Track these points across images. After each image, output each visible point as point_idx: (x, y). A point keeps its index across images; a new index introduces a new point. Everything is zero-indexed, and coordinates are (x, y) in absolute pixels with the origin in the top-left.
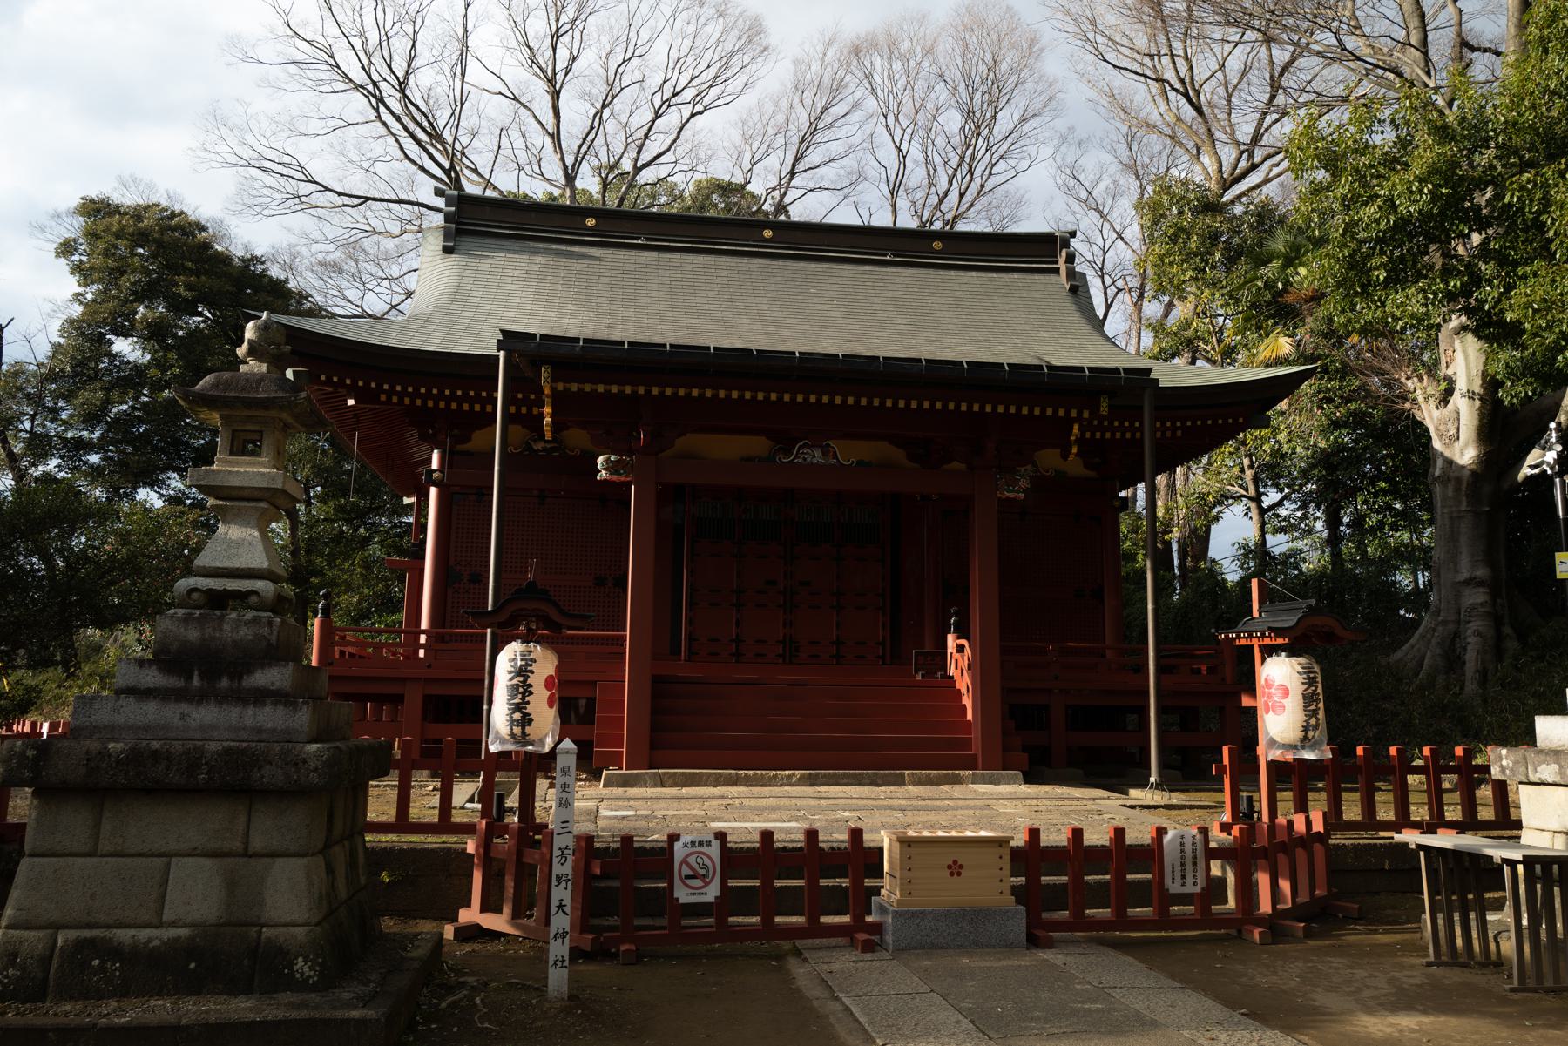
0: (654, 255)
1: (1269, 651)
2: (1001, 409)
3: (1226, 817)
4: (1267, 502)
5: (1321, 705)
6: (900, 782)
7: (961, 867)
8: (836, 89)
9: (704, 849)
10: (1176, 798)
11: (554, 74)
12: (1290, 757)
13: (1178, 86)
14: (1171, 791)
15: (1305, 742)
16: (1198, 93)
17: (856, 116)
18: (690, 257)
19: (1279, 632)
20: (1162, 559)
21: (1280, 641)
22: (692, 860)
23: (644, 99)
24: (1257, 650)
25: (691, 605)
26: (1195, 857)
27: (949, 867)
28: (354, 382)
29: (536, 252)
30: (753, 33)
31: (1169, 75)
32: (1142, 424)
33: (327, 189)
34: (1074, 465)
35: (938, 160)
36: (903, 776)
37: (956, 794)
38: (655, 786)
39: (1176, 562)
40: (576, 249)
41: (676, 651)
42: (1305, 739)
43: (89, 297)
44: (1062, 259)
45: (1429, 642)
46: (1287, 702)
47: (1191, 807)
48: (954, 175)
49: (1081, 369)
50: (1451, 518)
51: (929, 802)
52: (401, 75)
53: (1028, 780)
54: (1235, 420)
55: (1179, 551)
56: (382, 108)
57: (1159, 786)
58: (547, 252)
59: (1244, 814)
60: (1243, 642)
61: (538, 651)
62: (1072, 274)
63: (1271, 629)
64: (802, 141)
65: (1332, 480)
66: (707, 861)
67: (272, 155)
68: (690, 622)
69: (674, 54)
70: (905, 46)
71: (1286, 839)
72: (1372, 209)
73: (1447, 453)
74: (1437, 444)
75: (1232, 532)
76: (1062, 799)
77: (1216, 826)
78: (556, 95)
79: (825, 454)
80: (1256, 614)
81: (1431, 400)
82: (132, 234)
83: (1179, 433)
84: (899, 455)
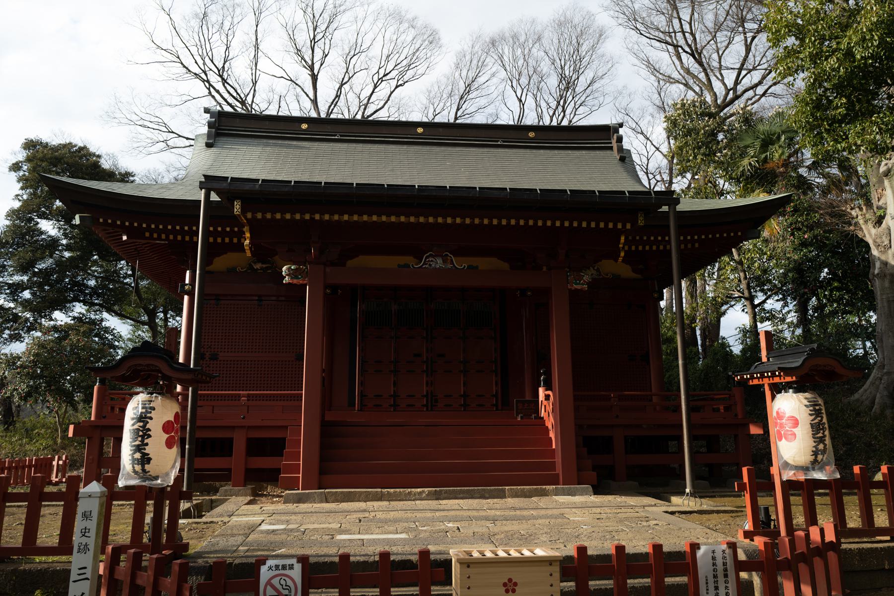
0: (345, 145)
1: (777, 389)
2: (567, 224)
3: (748, 526)
4: (756, 302)
5: (827, 433)
6: (502, 495)
7: (515, 584)
8: (481, 66)
9: (287, 572)
10: (706, 504)
11: (313, 64)
12: (802, 477)
13: (688, 49)
14: (701, 497)
15: (815, 464)
16: (700, 54)
17: (495, 80)
18: (369, 146)
19: (787, 371)
20: (689, 341)
21: (788, 379)
22: (275, 582)
23: (369, 80)
24: (767, 388)
25: (363, 371)
26: (726, 570)
27: (505, 585)
28: (123, 223)
29: (267, 145)
30: (433, 39)
31: (682, 42)
32: (670, 238)
33: (180, 136)
34: (624, 270)
35: (543, 105)
36: (504, 491)
37: (541, 505)
38: (321, 502)
39: (699, 342)
40: (295, 143)
41: (352, 404)
42: (815, 462)
43: (25, 197)
44: (614, 141)
45: (878, 388)
46: (798, 431)
47: (718, 512)
48: (554, 113)
49: (623, 192)
50: (888, 301)
51: (518, 512)
52: (220, 67)
53: (597, 491)
54: (736, 234)
55: (701, 335)
56: (211, 89)
57: (693, 494)
58: (275, 145)
59: (763, 524)
60: (756, 382)
61: (158, 401)
62: (621, 149)
63: (781, 369)
64: (461, 98)
65: (799, 284)
66: (289, 582)
67: (148, 117)
68: (361, 383)
69: (385, 52)
70: (522, 39)
71: (805, 550)
72: (833, 61)
73: (883, 258)
74: (875, 252)
75: (734, 321)
76: (620, 507)
77: (740, 535)
78: (314, 78)
79: (444, 262)
80: (764, 359)
81: (869, 223)
82: (51, 158)
83: (697, 245)
84: (505, 266)
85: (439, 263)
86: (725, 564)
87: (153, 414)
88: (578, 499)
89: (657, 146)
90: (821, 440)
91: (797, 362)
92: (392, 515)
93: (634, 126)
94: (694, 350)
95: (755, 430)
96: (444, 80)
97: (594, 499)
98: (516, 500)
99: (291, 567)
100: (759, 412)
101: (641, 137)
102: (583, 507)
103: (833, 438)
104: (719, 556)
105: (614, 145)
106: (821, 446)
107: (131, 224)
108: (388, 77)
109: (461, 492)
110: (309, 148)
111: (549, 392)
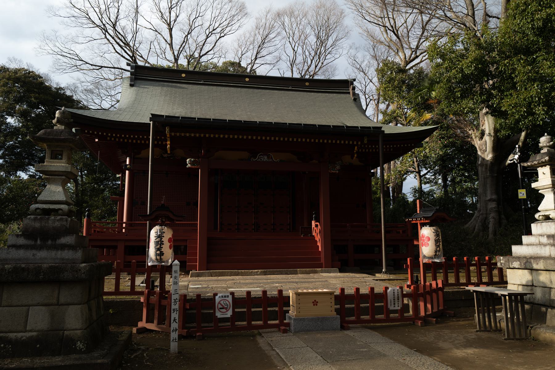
0: (207, 87)
1: (423, 225)
4: (422, 173)
5: (441, 243)
6: (296, 273)
7: (317, 302)
10: (392, 277)
11: (170, 22)
13: (391, 28)
15: (436, 256)
16: (397, 31)
18: (219, 88)
19: (426, 218)
20: (386, 193)
21: (427, 221)
22: (222, 302)
26: (398, 297)
27: (313, 302)
29: (164, 86)
31: (388, 24)
32: (379, 146)
33: (87, 63)
35: (307, 53)
36: (297, 271)
37: (315, 277)
39: (391, 195)
40: (179, 85)
44: (351, 89)
46: (430, 243)
47: (397, 280)
53: (341, 271)
56: (107, 34)
57: (386, 273)
58: (168, 86)
60: (414, 222)
61: (166, 229)
62: (354, 94)
63: (424, 217)
64: (259, 47)
65: (444, 165)
66: (227, 303)
67: (66, 50)
69: (213, 16)
73: (483, 156)
74: (479, 153)
75: (410, 183)
78: (171, 30)
79: (268, 158)
80: (418, 212)
82: (14, 78)
83: (392, 150)
85: (265, 158)
86: (398, 295)
87: (164, 235)
88: (332, 274)
89: (371, 83)
90: (438, 246)
91: (430, 214)
92: (247, 281)
93: (358, 66)
94: (388, 199)
95: (415, 243)
96: (248, 35)
97: (339, 274)
98: (303, 275)
99: (228, 296)
100: (416, 236)
101: (362, 73)
102: (335, 277)
103: (443, 245)
104: (396, 292)
105: (351, 91)
106: (438, 249)
107: (102, 134)
108: (215, 32)
109: (277, 271)
110: (186, 88)
111: (318, 223)
